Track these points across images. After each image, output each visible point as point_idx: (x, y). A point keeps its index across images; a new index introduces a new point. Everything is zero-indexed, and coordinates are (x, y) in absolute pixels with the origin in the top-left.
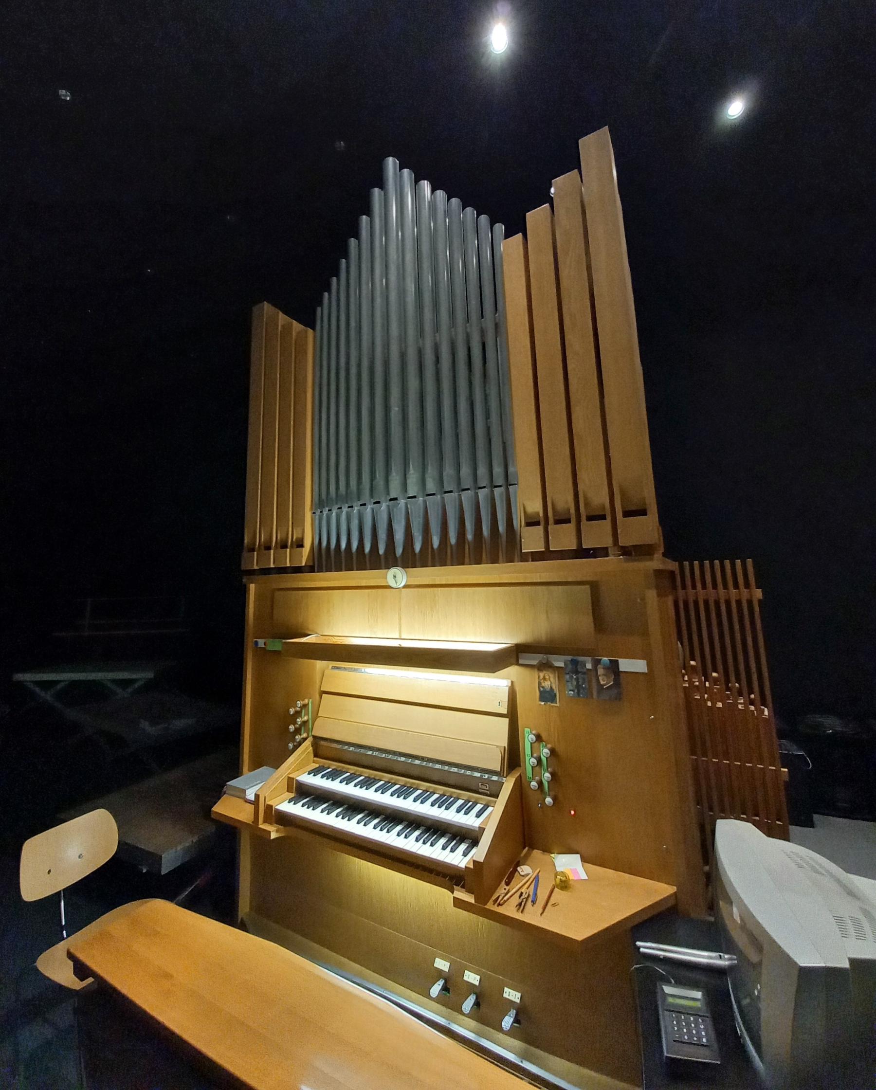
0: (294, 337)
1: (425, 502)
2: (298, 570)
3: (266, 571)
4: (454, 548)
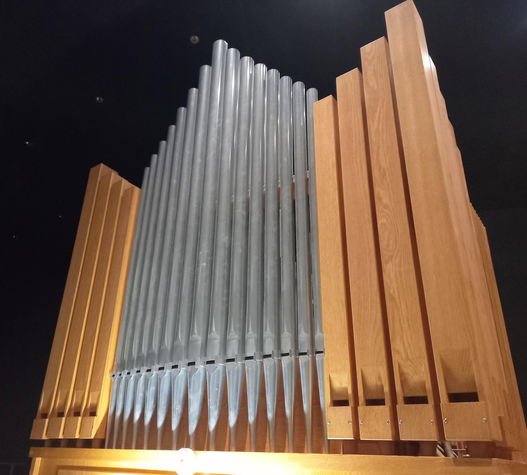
0: (121, 194)
1: (225, 368)
2: (88, 444)
3: (55, 443)
4: (232, 431)
